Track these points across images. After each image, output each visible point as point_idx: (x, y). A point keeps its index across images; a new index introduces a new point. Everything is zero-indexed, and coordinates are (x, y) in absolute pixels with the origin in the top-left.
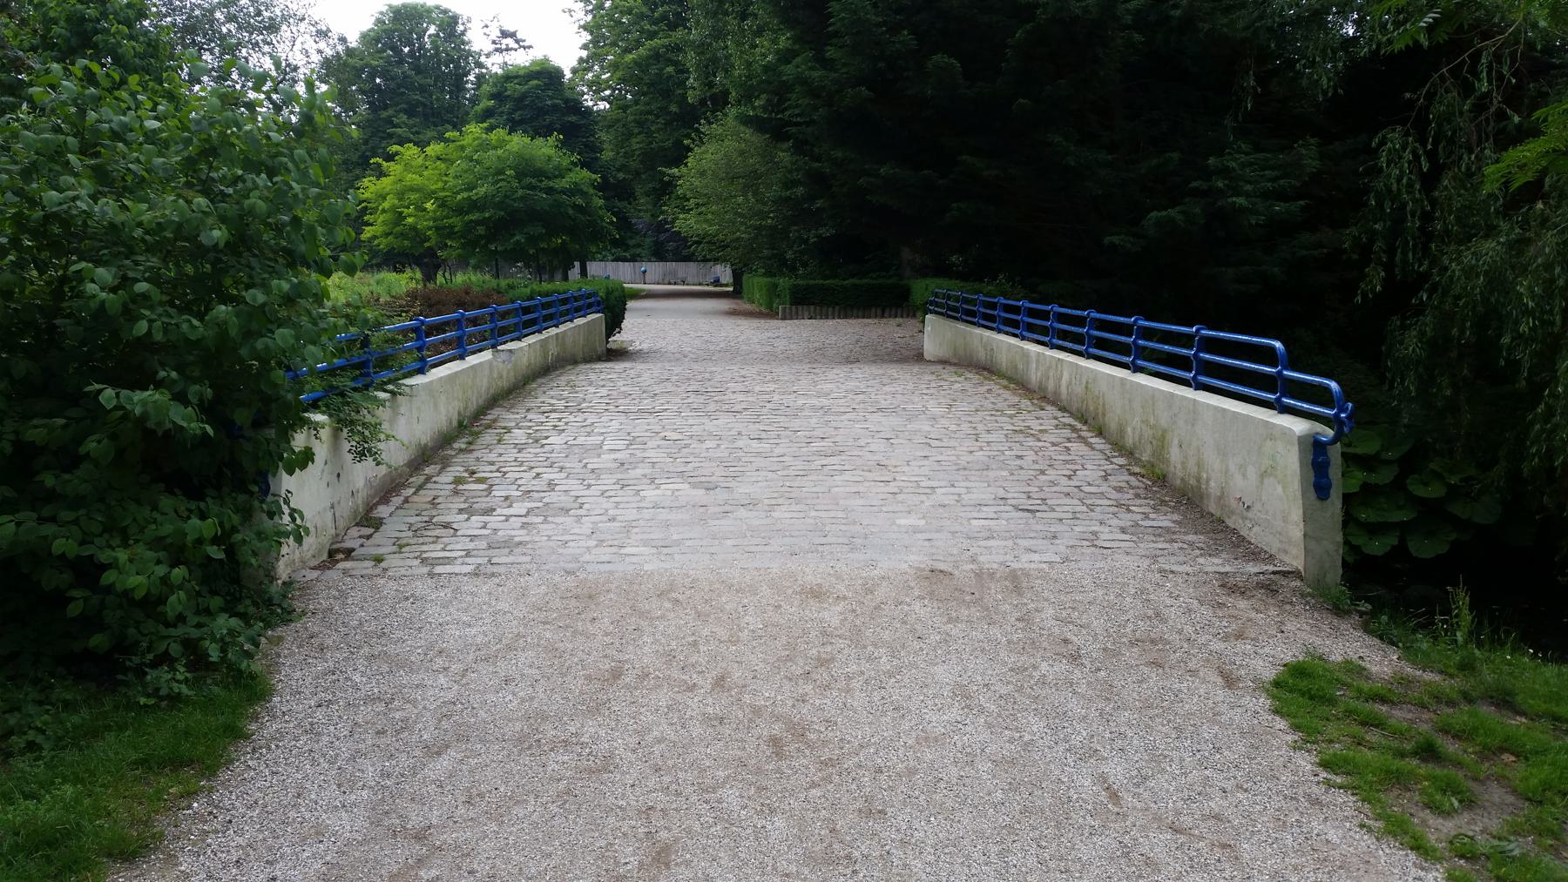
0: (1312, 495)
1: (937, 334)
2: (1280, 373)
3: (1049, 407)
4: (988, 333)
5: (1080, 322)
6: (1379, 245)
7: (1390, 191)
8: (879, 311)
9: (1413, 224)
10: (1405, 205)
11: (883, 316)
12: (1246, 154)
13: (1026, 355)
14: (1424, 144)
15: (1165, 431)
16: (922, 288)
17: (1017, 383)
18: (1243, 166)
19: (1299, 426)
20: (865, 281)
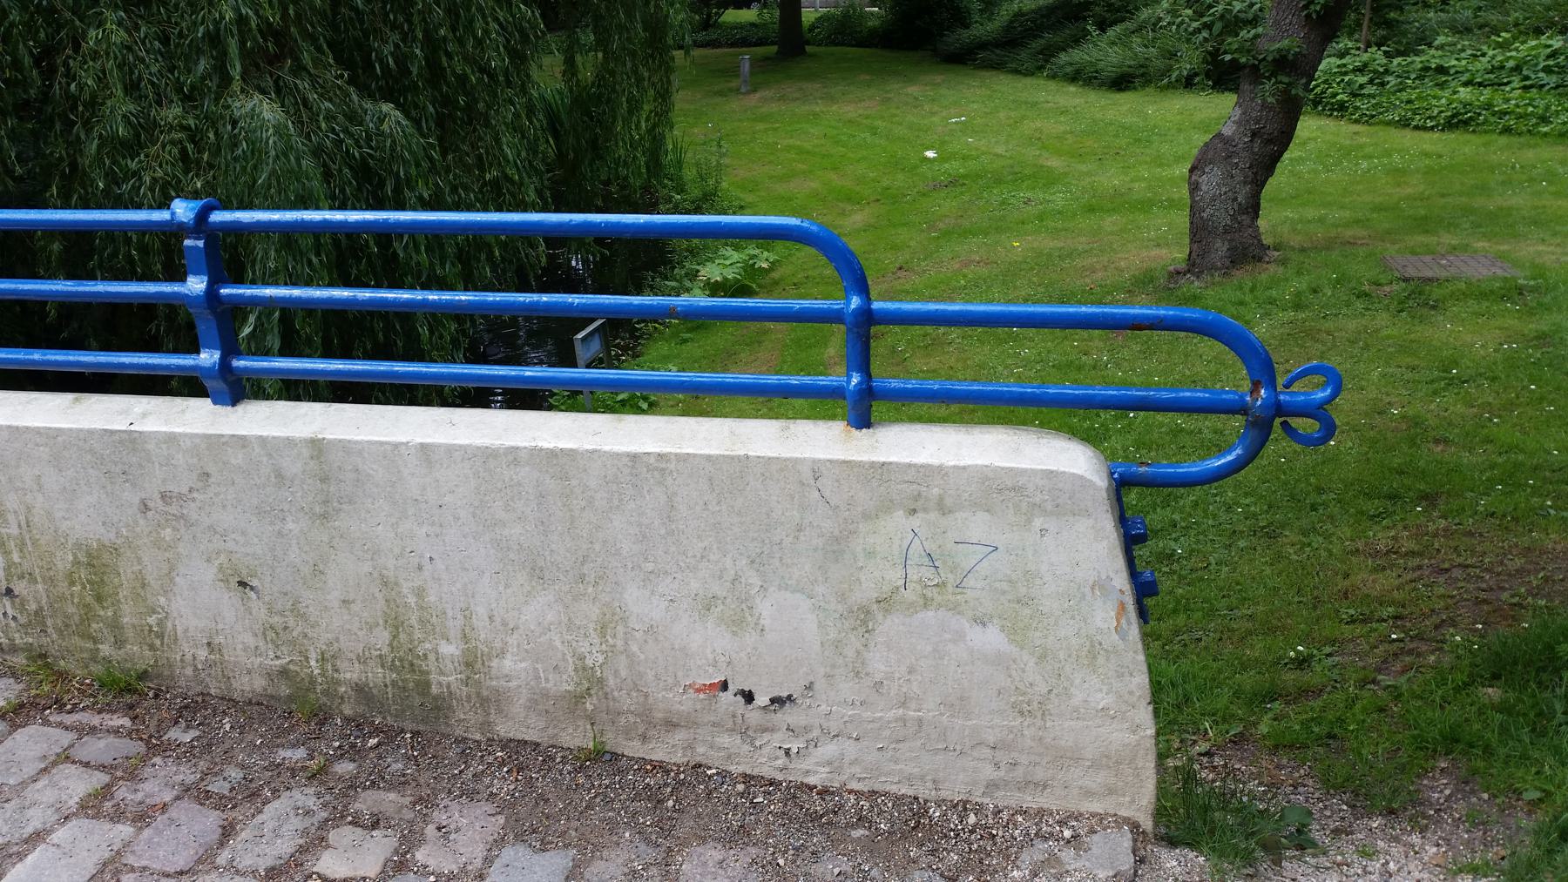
15: (96, 568)
19: (1072, 460)
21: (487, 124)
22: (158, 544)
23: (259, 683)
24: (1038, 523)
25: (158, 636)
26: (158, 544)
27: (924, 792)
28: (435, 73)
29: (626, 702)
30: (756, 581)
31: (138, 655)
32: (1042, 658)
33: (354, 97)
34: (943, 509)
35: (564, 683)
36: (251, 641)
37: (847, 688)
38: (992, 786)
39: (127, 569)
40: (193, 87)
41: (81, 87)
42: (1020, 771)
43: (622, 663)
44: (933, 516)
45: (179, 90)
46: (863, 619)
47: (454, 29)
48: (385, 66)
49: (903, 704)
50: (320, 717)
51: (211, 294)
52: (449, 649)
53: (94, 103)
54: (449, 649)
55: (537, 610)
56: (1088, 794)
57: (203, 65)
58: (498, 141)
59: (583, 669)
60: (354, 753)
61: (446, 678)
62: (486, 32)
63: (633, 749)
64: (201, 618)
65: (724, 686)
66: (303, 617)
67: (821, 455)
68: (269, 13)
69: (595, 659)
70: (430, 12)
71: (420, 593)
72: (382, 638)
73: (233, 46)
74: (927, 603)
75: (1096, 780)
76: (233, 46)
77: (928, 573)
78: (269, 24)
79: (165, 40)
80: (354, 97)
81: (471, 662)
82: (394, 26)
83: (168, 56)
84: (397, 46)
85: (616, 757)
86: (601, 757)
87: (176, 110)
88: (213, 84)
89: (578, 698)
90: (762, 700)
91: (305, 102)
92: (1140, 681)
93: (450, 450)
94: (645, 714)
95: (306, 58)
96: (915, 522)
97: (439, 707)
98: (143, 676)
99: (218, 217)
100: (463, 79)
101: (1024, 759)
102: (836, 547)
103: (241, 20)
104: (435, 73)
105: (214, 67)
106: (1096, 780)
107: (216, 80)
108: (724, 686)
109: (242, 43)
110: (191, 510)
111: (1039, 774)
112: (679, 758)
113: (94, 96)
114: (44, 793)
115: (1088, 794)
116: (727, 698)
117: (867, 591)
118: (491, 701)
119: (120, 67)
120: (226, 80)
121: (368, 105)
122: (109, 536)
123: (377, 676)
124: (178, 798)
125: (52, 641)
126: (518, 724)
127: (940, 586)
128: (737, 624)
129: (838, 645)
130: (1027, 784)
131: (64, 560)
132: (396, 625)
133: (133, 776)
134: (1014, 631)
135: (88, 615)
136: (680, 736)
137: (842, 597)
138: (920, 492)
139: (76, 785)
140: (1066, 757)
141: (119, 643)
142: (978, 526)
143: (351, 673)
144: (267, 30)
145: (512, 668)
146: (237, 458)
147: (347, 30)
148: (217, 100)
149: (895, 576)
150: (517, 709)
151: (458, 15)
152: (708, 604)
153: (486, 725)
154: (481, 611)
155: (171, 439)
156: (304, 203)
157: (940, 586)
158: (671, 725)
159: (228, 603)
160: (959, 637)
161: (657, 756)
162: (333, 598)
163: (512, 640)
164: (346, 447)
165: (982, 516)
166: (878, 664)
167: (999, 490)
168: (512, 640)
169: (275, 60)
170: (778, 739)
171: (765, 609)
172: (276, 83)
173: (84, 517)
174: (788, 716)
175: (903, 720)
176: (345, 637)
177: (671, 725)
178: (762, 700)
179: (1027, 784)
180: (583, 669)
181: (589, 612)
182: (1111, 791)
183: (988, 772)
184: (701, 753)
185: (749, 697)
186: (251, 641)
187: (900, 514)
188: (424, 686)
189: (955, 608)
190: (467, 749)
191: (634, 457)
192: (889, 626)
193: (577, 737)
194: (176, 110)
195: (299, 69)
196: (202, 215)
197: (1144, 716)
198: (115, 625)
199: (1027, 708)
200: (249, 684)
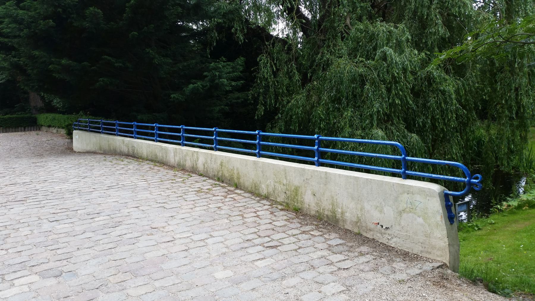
0: (449, 223)
1: (81, 139)
2: (404, 158)
3: (193, 175)
4: (128, 139)
5: (178, 131)
6: (261, 98)
7: (264, 77)
8: (23, 128)
9: (272, 90)
10: (269, 82)
11: (25, 131)
12: (224, 62)
13: (166, 150)
14: (273, 61)
15: (297, 189)
16: (42, 118)
17: (158, 162)
18: (223, 67)
19: (436, 188)
20: (15, 116)
21: (449, 143)
22: (305, 187)
23: (314, 213)
24: (428, 198)
25: (302, 202)
26: (305, 187)
27: (410, 251)
28: (434, 127)
29: (364, 225)
30: (384, 204)
31: (299, 205)
32: (429, 225)
33: (406, 132)
34: (413, 194)
35: (355, 219)
36: (314, 205)
37: (398, 227)
38: (422, 252)
39: (300, 190)
40: (365, 127)
41: (341, 125)
42: (426, 249)
43: (364, 217)
44: (411, 195)
45: (362, 127)
46: (400, 213)
47: (442, 116)
48: (419, 125)
49: (407, 232)
50: (321, 220)
51: (318, 149)
52: (340, 210)
53: (342, 129)
54: (340, 210)
55: (352, 205)
56: (438, 256)
57: (367, 122)
58: (452, 148)
59: (358, 217)
60: (324, 225)
61: (339, 216)
62: (452, 117)
63: (365, 234)
64: (309, 201)
65: (378, 224)
66: (321, 201)
67: (395, 182)
68: (385, 110)
69: (360, 215)
70: (434, 111)
71: (337, 199)
72: (331, 207)
73: (375, 117)
74: (410, 212)
75: (439, 253)
76: (375, 117)
77: (410, 206)
78: (386, 113)
79: (361, 116)
80: (406, 132)
81: (342, 213)
82: (424, 115)
83: (361, 119)
84: (423, 120)
85: (361, 235)
86: (359, 234)
87: (360, 132)
88: (369, 126)
89: (357, 222)
90: (384, 227)
91: (392, 132)
92: (445, 232)
93: (343, 175)
94: (366, 227)
95: (395, 122)
96: (408, 196)
97: (337, 221)
98: (300, 209)
99: (320, 138)
100: (442, 129)
101: (427, 247)
102: (396, 199)
103: (378, 112)
104: (434, 127)
105: (370, 122)
106: (439, 253)
107: (370, 125)
108: (378, 224)
109: (378, 117)
110: (309, 182)
111: (429, 250)
112: (371, 237)
113: (343, 127)
114: (281, 217)
115: (438, 256)
116: (379, 226)
117: (401, 208)
118: (344, 221)
119: (349, 121)
120: (372, 125)
121: (409, 134)
122: (299, 185)
123: (330, 214)
124: (301, 233)
125: (289, 202)
126: (348, 226)
127: (412, 209)
128: (381, 212)
129: (396, 218)
130: (427, 252)
131: (293, 188)
132: (333, 205)
133: (293, 219)
134: (425, 219)
135: (294, 198)
136: (372, 233)
137: (397, 209)
138: (409, 191)
139: (285, 218)
140: (433, 247)
141: (297, 203)
142: (418, 198)
143: (326, 213)
144: (385, 114)
145: (348, 215)
146: (316, 174)
147: (410, 115)
148: (369, 130)
149: (405, 206)
150: (348, 223)
151: (444, 112)
152: (377, 207)
153: (344, 226)
154: (344, 204)
155: (309, 170)
156: (387, 153)
157: (412, 209)
158: (370, 230)
159: (312, 197)
160: (416, 219)
161: (368, 236)
162: (325, 199)
163: (348, 210)
164: (329, 173)
165: (419, 196)
166: (403, 223)
167: (422, 191)
168: (348, 210)
169: (388, 121)
170: (387, 236)
171: (385, 209)
172: (386, 127)
173: (296, 181)
174: (388, 232)
175: (406, 235)
176: (326, 207)
177: (370, 230)
178: (384, 227)
179: (427, 252)
180: (358, 217)
181: (359, 206)
182: (442, 256)
183: (421, 249)
184: (375, 237)
185: (382, 226)
186: (314, 205)
187: (406, 194)
188: (336, 216)
189: (415, 213)
190: (340, 229)
191: (367, 179)
192: (404, 215)
193: (356, 230)
194: (360, 132)
195: (392, 124)
196: (318, 137)
197: (446, 240)
198: (297, 200)
199: (427, 236)
200: (313, 213)
